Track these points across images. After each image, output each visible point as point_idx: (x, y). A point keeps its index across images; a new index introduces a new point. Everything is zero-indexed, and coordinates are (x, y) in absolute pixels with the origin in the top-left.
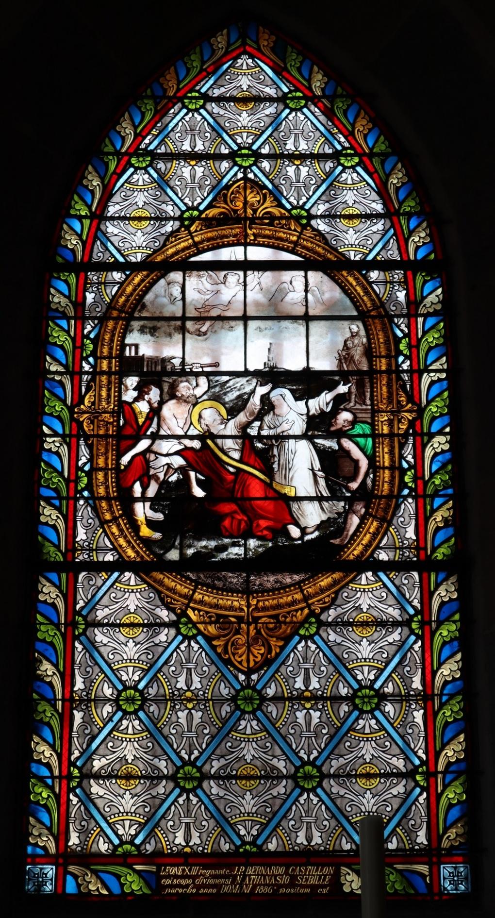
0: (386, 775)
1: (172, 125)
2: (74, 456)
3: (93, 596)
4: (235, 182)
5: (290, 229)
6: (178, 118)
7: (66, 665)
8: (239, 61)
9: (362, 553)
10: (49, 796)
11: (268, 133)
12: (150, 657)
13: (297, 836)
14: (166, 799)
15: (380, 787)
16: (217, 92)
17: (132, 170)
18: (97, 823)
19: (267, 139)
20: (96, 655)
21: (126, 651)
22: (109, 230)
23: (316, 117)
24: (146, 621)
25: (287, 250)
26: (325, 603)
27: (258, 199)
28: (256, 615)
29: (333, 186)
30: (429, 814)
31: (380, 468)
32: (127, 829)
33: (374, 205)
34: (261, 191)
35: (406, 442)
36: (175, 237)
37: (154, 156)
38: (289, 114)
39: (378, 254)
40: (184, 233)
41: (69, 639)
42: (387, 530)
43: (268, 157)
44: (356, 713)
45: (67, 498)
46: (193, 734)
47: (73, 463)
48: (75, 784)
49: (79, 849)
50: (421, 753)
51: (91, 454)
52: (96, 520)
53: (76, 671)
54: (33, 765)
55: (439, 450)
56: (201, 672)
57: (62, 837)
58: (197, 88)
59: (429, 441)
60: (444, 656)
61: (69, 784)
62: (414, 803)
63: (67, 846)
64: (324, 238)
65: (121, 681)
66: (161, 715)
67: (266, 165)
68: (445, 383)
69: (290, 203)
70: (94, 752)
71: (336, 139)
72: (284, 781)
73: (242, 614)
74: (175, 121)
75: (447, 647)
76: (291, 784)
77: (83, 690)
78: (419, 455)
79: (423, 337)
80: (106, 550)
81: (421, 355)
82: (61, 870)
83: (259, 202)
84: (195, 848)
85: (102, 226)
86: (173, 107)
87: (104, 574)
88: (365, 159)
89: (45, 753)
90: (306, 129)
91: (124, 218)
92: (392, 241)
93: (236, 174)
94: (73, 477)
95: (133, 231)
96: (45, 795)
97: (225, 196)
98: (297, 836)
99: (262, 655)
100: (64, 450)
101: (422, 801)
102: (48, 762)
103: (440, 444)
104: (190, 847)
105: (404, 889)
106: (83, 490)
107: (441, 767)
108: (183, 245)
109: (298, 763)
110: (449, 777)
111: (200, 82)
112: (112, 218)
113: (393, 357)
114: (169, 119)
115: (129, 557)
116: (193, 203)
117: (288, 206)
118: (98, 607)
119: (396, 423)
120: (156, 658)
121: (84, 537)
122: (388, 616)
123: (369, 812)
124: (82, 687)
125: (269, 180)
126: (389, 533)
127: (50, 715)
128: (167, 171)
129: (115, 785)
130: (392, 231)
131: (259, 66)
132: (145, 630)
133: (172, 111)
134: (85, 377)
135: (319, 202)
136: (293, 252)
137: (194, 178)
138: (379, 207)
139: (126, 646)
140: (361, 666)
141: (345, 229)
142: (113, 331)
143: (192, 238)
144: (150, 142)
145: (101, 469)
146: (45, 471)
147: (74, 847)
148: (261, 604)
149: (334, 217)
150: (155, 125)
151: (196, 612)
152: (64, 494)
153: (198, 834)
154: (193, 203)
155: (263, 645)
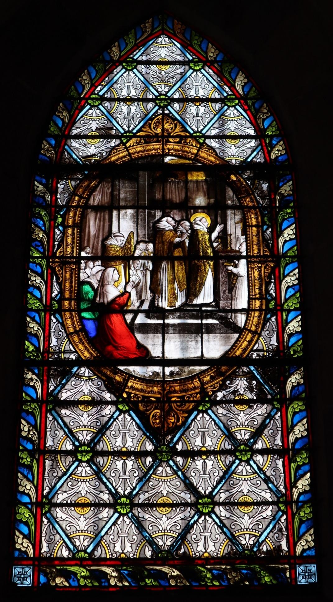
0: (258, 504)
1: (116, 78)
2: (49, 289)
3: (56, 484)
4: (156, 117)
5: (192, 145)
6: (120, 74)
9: (241, 354)
11: (177, 86)
12: (98, 424)
15: (254, 511)
16: (144, 58)
17: (88, 107)
19: (178, 89)
20: (57, 526)
21: (83, 420)
23: (210, 75)
27: (172, 126)
29: (221, 118)
31: (249, 226)
32: (85, 437)
33: (248, 131)
34: (174, 122)
37: (102, 99)
38: (193, 73)
40: (122, 147)
42: (258, 339)
44: (237, 462)
46: (131, 117)
51: (61, 288)
52: (64, 332)
53: (48, 433)
54: (31, 264)
55: (291, 284)
56: (131, 540)
58: (131, 56)
61: (47, 408)
63: (45, 447)
64: (215, 151)
66: (105, 464)
68: (295, 241)
69: (192, 129)
71: (223, 89)
74: (118, 76)
75: (290, 290)
77: (56, 346)
78: (278, 290)
80: (71, 353)
81: (292, 470)
83: (172, 128)
84: (128, 554)
85: (69, 143)
86: (116, 68)
90: (202, 83)
91: (69, 505)
92: (260, 153)
93: (157, 111)
94: (48, 304)
96: (28, 487)
97: (150, 125)
99: (173, 423)
101: (283, 521)
103: (289, 235)
104: (124, 553)
105: (271, 581)
108: (121, 155)
111: (134, 51)
112: (61, 505)
114: (113, 75)
115: (85, 357)
117: (192, 132)
118: (59, 492)
119: (263, 268)
120: (100, 529)
121: (56, 344)
123: (241, 380)
124: (47, 550)
125: (179, 115)
126: (259, 341)
127: (29, 488)
128: (112, 108)
129: (73, 512)
130: (259, 148)
131: (173, 43)
132: (92, 509)
133: (115, 71)
135: (212, 128)
137: (130, 112)
138: (252, 132)
139: (82, 417)
140: (244, 534)
141: (238, 412)
143: (128, 151)
144: (101, 90)
145: (67, 299)
147: (54, 348)
148: (173, 388)
149: (233, 504)
150: (104, 79)
155: (174, 416)
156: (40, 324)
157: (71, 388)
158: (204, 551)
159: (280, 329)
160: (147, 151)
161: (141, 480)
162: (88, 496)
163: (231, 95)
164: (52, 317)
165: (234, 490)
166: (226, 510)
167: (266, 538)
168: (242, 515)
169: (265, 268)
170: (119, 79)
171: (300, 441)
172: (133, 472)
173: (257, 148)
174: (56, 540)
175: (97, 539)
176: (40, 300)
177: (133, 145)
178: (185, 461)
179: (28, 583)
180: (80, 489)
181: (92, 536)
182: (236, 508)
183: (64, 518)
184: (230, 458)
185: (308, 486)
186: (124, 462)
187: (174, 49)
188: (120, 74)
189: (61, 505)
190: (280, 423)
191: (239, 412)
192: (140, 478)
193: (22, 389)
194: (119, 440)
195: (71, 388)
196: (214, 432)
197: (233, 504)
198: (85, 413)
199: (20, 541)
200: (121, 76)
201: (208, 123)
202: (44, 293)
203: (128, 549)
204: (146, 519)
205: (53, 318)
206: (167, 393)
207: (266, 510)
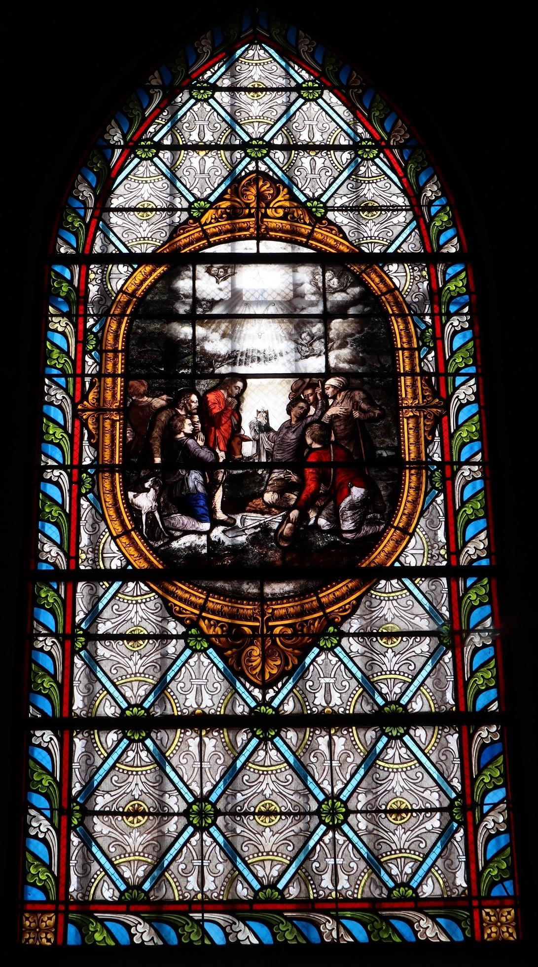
7: (64, 771)
10: (51, 739)
13: (315, 697)
15: (384, 216)
17: (136, 160)
18: (104, 686)
25: (301, 244)
26: (345, 610)
28: (270, 624)
30: (467, 854)
35: (432, 441)
36: (184, 229)
39: (399, 247)
41: (69, 654)
43: (281, 148)
45: (74, 376)
48: (91, 348)
50: (456, 783)
54: (45, 408)
57: (65, 786)
59: (458, 470)
60: (456, 345)
67: (279, 155)
72: (174, 641)
73: (258, 624)
74: (184, 109)
79: (460, 508)
81: (454, 453)
82: (61, 918)
87: (105, 583)
89: (43, 782)
92: (413, 233)
98: (315, 697)
100: (57, 652)
102: (52, 608)
113: (415, 349)
116: (199, 658)
130: (414, 224)
134: (87, 379)
136: (306, 245)
141: (383, 650)
142: (114, 388)
146: (54, 281)
151: (206, 621)
152: (70, 371)
154: (199, 658)
156: (60, 546)
163: (368, 140)
165: (381, 789)
169: (425, 417)
170: (185, 114)
171: (488, 748)
172: (216, 757)
174: (93, 872)
175: (158, 869)
178: (301, 736)
179: (47, 939)
183: (108, 656)
186: (199, 706)
187: (274, 68)
188: (188, 106)
189: (101, 813)
190: (463, 847)
193: (40, 447)
194: (191, 697)
196: (345, 683)
197: (370, 635)
200: (188, 110)
201: (330, 185)
202: (57, 702)
204: (238, 835)
206: (269, 620)
207: (420, 643)
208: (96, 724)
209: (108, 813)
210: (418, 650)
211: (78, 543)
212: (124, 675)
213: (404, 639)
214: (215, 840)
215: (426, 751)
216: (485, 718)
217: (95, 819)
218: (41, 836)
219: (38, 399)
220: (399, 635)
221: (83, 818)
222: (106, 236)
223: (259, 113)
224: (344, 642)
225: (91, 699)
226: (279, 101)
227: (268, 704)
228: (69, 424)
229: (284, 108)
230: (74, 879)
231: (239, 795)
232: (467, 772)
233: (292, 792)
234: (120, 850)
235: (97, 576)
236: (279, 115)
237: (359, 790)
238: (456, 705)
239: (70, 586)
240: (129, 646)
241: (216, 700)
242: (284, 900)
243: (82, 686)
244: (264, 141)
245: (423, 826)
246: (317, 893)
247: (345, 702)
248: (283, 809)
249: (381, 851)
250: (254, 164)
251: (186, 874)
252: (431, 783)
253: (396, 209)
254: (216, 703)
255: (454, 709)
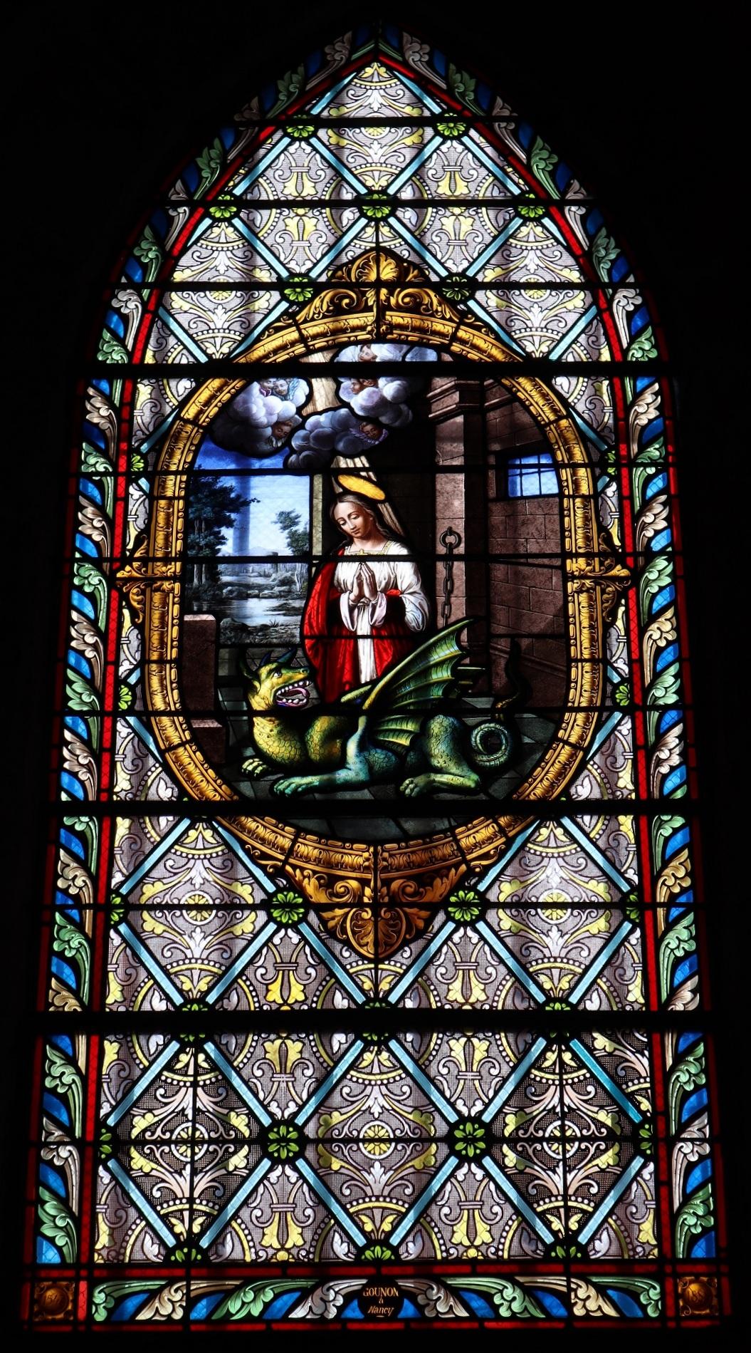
8: (368, 69)
14: (249, 1175)
18: (179, 340)
22: (147, 927)
24: (217, 902)
29: (504, 246)
33: (566, 273)
47: (91, 1113)
49: (130, 795)
50: (631, 874)
62: (634, 1179)
63: (104, 1005)
65: (180, 991)
70: (135, 1104)
76: (444, 1149)
88: (553, 210)
90: (464, 163)
94: (90, 1137)
95: (211, 306)
101: (647, 1176)
106: (119, 906)
107: (662, 895)
109: (453, 1118)
110: (675, 912)
116: (283, 1171)
120: (228, 1194)
122: (590, 894)
131: (397, 77)
138: (575, 276)
153: (300, 1230)
154: (283, 1171)
157: (192, 262)
158: (467, 1243)
159: (634, 636)
160: (343, 331)
161: (320, 1083)
162: (230, 273)
164: (101, 1168)
166: (513, 917)
167: (598, 976)
168: (527, 305)
173: (587, 311)
176: (76, 993)
177: (313, 319)
180: (216, 263)
181: (215, 970)
182: (533, 912)
184: (504, 215)
185: (692, 942)
189: (151, 908)
190: (653, 1189)
191: (548, 927)
192: (317, 1080)
195: (192, 262)
198: (198, 930)
199: (56, 1071)
203: (295, 1238)
205: (112, 934)
208: (135, 1024)
209: (161, 907)
210: (570, 306)
211: (94, 1242)
212: (180, 955)
213: (575, 913)
214: (301, 1176)
215: (592, 835)
216: (668, 805)
217: (145, 915)
218: (87, 589)
219: (63, 586)
220: (563, 903)
221: (126, 914)
222: (166, 325)
223: (379, 156)
224: (491, 915)
225: (130, 988)
226: (409, 141)
227: (385, 1243)
228: (110, 502)
229: (414, 152)
230: (103, 1228)
231: (336, 1114)
232: (664, 1206)
233: (410, 1110)
234: (203, 327)
235: (141, 809)
236: (408, 161)
237: (503, 878)
238: (636, 790)
239: (129, 385)
240: (187, 907)
241: (320, 187)
242: (397, 1261)
243: (128, 762)
244: (388, 195)
245: (594, 1163)
246: (447, 1251)
247: (491, 996)
248: (398, 1132)
249: (530, 959)
250: (370, 231)
251: (262, 1225)
252: (596, 872)
253: (570, 286)
254: (320, 191)
255: (633, 796)
